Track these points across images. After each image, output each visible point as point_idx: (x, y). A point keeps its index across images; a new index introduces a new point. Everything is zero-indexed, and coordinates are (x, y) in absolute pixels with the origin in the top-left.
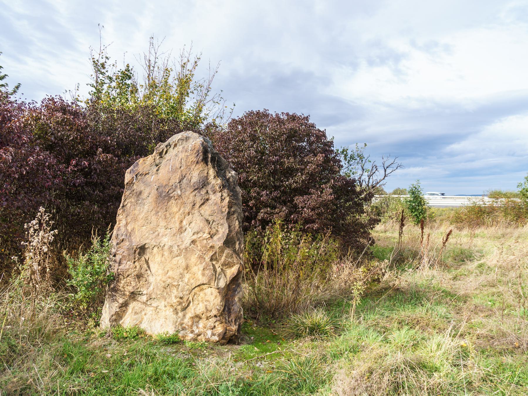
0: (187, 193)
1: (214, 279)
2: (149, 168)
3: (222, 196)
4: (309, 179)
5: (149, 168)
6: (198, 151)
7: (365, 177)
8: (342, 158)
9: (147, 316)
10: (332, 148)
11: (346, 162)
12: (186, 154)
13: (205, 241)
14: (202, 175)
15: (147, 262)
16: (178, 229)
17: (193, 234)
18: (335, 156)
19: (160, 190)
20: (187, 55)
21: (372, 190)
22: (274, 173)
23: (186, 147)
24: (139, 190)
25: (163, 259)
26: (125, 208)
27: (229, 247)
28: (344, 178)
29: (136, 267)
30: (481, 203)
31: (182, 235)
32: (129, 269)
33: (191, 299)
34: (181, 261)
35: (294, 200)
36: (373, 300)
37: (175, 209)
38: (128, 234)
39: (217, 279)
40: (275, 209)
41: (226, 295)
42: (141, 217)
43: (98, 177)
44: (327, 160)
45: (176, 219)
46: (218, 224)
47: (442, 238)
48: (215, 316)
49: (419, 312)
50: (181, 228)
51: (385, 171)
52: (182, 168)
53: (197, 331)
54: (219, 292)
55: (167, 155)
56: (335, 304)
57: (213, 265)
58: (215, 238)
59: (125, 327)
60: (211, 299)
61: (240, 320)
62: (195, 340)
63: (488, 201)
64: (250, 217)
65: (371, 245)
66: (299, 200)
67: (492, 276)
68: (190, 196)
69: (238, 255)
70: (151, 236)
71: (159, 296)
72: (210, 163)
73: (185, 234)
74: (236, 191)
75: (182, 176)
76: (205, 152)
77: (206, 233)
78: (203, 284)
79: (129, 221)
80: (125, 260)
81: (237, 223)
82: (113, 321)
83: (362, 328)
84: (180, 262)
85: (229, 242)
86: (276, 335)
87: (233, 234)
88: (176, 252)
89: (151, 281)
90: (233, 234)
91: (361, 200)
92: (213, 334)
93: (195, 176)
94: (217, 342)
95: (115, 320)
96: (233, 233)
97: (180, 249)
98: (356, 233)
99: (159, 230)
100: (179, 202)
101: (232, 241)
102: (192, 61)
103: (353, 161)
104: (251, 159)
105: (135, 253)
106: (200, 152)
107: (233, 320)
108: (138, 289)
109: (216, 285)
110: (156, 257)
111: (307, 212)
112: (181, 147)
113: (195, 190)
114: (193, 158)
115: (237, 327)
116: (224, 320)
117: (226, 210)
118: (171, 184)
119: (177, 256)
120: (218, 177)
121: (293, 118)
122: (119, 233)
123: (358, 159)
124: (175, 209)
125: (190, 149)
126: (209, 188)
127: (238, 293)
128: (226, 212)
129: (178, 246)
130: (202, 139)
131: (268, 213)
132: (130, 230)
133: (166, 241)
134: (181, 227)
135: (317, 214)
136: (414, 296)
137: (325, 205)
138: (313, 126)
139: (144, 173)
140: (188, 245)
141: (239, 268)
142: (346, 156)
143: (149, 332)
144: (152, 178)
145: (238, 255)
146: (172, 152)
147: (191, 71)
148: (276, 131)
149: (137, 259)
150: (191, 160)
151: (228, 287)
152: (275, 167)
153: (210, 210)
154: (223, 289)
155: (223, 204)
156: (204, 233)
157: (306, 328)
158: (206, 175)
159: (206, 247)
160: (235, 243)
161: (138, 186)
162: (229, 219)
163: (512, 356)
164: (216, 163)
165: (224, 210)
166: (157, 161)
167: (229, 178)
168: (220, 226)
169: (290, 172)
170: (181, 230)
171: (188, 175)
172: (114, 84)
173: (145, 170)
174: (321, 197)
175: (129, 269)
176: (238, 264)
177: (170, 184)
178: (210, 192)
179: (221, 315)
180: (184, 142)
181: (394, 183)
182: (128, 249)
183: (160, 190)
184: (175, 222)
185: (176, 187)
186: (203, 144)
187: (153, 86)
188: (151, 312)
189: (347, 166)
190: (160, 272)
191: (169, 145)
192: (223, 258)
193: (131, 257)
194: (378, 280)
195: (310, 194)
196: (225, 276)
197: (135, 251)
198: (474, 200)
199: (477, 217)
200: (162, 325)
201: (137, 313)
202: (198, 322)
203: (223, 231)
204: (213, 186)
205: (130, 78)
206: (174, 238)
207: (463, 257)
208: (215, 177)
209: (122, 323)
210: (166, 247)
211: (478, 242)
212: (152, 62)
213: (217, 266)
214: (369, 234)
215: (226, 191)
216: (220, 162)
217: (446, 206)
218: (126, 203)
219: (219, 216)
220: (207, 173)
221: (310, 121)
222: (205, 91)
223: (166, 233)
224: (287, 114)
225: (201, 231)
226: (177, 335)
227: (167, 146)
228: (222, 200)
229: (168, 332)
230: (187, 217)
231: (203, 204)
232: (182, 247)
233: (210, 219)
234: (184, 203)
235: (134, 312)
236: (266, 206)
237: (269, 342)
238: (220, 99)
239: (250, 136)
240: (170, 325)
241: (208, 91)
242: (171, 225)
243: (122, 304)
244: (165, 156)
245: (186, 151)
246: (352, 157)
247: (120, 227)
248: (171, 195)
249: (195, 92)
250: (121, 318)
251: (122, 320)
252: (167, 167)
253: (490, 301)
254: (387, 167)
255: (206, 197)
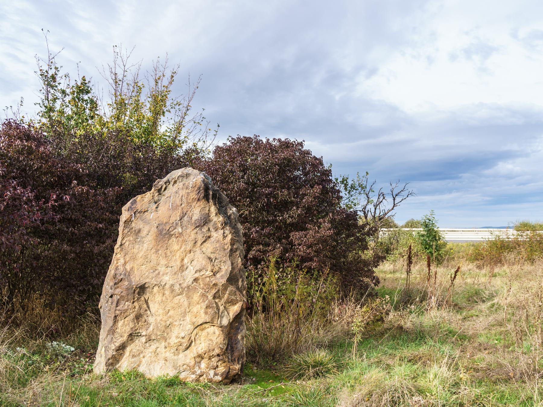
0: (188, 231)
1: (217, 317)
2: (148, 205)
3: (224, 233)
4: (306, 213)
5: (148, 205)
6: (199, 188)
7: (371, 207)
8: (341, 187)
9: (146, 359)
10: (330, 178)
11: (346, 193)
12: (187, 191)
13: (208, 279)
14: (203, 212)
15: (147, 302)
16: (179, 267)
17: (196, 272)
18: (334, 186)
19: (160, 228)
20: (162, 69)
21: (379, 222)
22: (267, 207)
23: (186, 184)
24: (137, 228)
25: (164, 298)
26: (123, 246)
27: (232, 284)
28: (343, 211)
29: (135, 307)
30: (505, 237)
31: (183, 274)
32: (127, 310)
33: (193, 338)
34: (182, 299)
35: (289, 237)
36: (377, 340)
37: (176, 247)
38: (127, 274)
39: (221, 317)
40: (269, 246)
41: (229, 333)
42: (140, 255)
43: (72, 213)
44: (325, 191)
45: (177, 257)
46: (220, 262)
47: (449, 276)
48: (218, 355)
49: (423, 349)
50: (183, 266)
51: (394, 200)
52: (183, 206)
53: (198, 372)
54: (222, 331)
55: (166, 191)
56: (338, 345)
57: (216, 303)
58: (218, 275)
59: (122, 371)
60: (212, 338)
61: (243, 359)
62: (197, 380)
63: (512, 234)
64: (251, 255)
65: (375, 285)
66: (295, 236)
67: (502, 315)
68: (191, 234)
69: (241, 292)
70: (151, 275)
71: (159, 337)
72: (211, 201)
73: (187, 272)
74: (237, 228)
75: (183, 213)
76: (206, 189)
77: (209, 270)
78: (206, 323)
79: (127, 259)
80: (123, 300)
81: (240, 260)
82: (109, 366)
83: (365, 363)
84: (182, 301)
85: (232, 279)
86: (278, 376)
87: (236, 271)
88: (177, 291)
89: (151, 321)
90: (236, 271)
91: (363, 234)
92: (216, 374)
93: (196, 213)
94: (220, 382)
95: (112, 364)
96: (236, 270)
97: (182, 288)
98: (359, 271)
99: (160, 269)
100: (180, 239)
101: (234, 279)
102: (168, 74)
103: (354, 191)
104: (241, 192)
105: (134, 293)
106: (201, 189)
107: (236, 359)
108: (136, 330)
109: (219, 323)
110: (156, 297)
111: (302, 250)
112: (181, 184)
113: (197, 227)
114: (194, 195)
115: (240, 365)
116: (227, 360)
117: (228, 247)
118: (171, 222)
119: (179, 295)
120: (220, 214)
121: (286, 145)
122: (118, 272)
123: (360, 189)
124: (176, 247)
125: (191, 186)
126: (211, 225)
127: (241, 331)
128: (229, 250)
129: (180, 284)
130: (203, 176)
131: (260, 252)
132: (128, 270)
133: (167, 279)
134: (183, 266)
135: (315, 251)
136: (419, 336)
137: (323, 241)
138: (308, 153)
139: (143, 210)
140: (190, 283)
141: (242, 305)
142: (346, 185)
143: (148, 376)
144: (151, 216)
145: (241, 292)
146: (172, 189)
147: (167, 87)
148: (267, 162)
149: (136, 299)
150: (192, 197)
151: (231, 324)
152: (268, 200)
153: (212, 248)
154: (226, 327)
155: (226, 241)
156: (207, 270)
157: (309, 367)
158: (207, 212)
159: (209, 285)
160: (238, 280)
161: (136, 224)
162: (231, 256)
163: (506, 385)
164: (217, 200)
165: (226, 247)
166: (156, 198)
167: (231, 215)
168: (222, 264)
169: (285, 206)
170: (183, 268)
171: (189, 212)
172: (68, 99)
173: (144, 208)
174: (318, 232)
175: (127, 310)
176: (241, 301)
177: (171, 221)
178: (211, 229)
179: (224, 354)
180: (185, 179)
181: (405, 214)
182: (127, 289)
183: (160, 228)
184: (176, 260)
185: (177, 224)
186: (204, 181)
187: (121, 105)
188: (150, 354)
189: (347, 196)
190: (161, 311)
191: (168, 182)
192: (226, 296)
193: (129, 297)
194: (382, 320)
195: (306, 229)
196: (228, 313)
197: (135, 291)
198: (497, 233)
199: (495, 253)
200: (161, 368)
201: (135, 356)
202: (200, 362)
203: (226, 268)
204: (215, 223)
205: (88, 92)
206: (176, 277)
207: (475, 297)
208: (216, 214)
209: (119, 367)
210: (167, 286)
211: (498, 282)
212: (120, 77)
213: (220, 304)
214: (373, 272)
215: (228, 228)
216: (221, 199)
217: (466, 241)
218: (124, 242)
219: (222, 253)
220: (209, 210)
221: (305, 148)
222: (184, 110)
223: (167, 271)
224: (279, 140)
225: (203, 269)
226: (177, 377)
227: (166, 183)
228: (225, 237)
229: (168, 374)
230: (188, 255)
231: (204, 242)
232: (185, 285)
233: (212, 256)
234: (184, 241)
235: (131, 355)
236: (259, 244)
237: (272, 382)
238: (202, 119)
239: (239, 166)
240: (170, 367)
241: (188, 110)
242: (172, 264)
243: (119, 347)
244: (164, 193)
245: (187, 188)
246: (353, 187)
247: (118, 266)
248: (172, 233)
249: (173, 111)
250: (118, 361)
251: (119, 364)
252: (167, 204)
253: (497, 340)
254: (396, 195)
255: (208, 235)
